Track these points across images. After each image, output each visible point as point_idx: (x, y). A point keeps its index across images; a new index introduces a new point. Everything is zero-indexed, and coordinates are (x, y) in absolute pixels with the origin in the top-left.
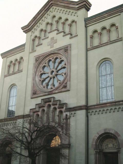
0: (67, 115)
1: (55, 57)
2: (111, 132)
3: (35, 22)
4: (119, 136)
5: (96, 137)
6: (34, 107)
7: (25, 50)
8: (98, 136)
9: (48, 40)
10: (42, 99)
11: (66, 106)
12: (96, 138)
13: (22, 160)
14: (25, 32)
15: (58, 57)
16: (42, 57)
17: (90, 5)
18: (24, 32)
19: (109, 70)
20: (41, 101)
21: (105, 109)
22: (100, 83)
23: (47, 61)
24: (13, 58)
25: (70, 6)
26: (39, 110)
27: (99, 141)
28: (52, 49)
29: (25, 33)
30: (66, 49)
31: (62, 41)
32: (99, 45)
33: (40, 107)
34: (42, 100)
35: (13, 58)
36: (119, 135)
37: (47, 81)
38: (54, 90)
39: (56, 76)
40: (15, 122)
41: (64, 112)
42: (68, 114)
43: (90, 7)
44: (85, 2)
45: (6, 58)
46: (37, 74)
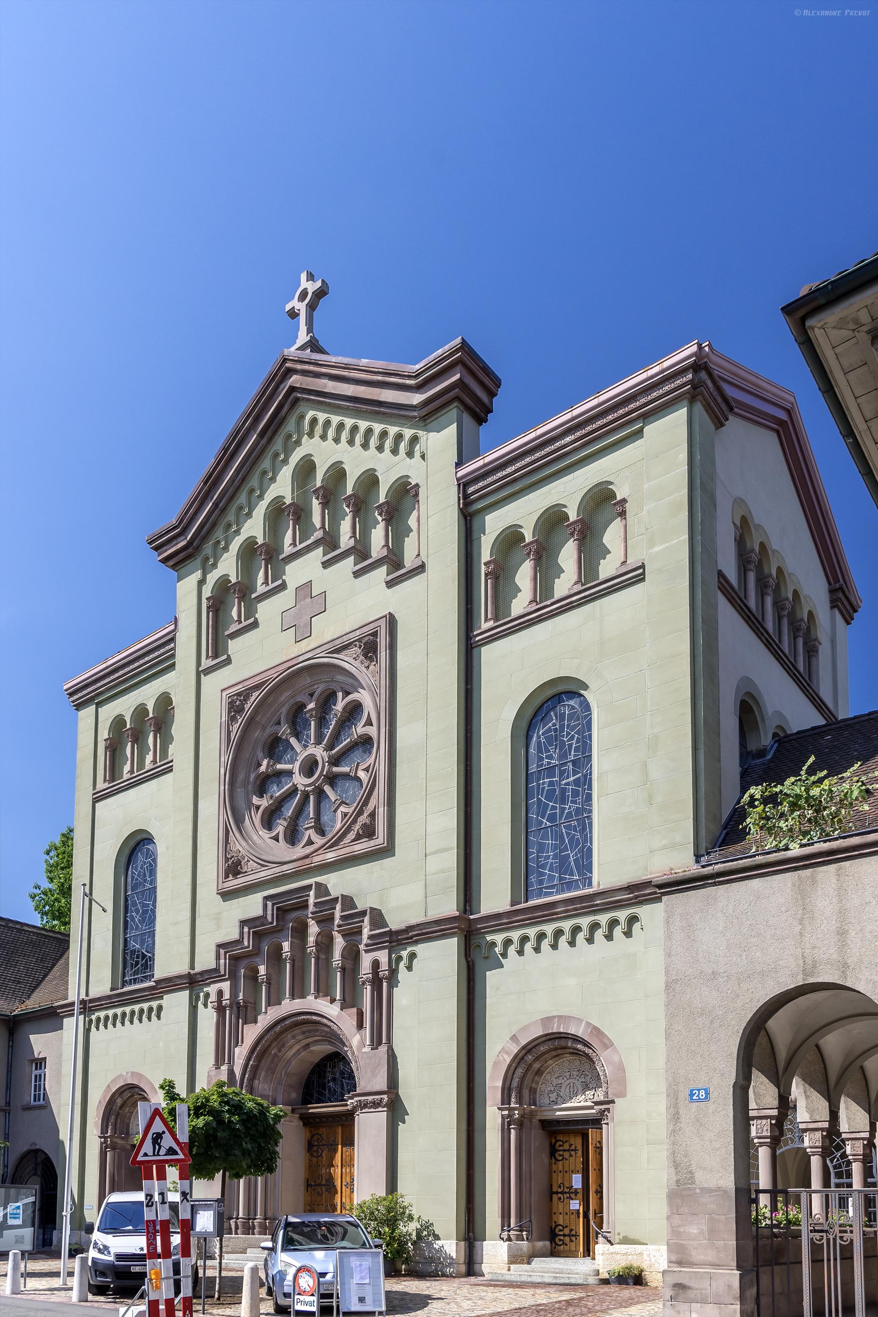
0: (376, 964)
1: (319, 689)
2: (572, 1030)
3: (216, 505)
4: (608, 1044)
5: (507, 1053)
6: (235, 936)
7: (178, 659)
8: (515, 1049)
9: (284, 600)
10: (76, 835)
11: (374, 925)
12: (508, 1061)
13: (229, 1250)
14: (171, 563)
15: (334, 686)
16: (257, 693)
17: (498, 383)
18: (164, 561)
19: (572, 738)
20: (265, 907)
21: (549, 929)
22: (530, 807)
23: (284, 710)
24: (124, 706)
25: (382, 398)
26: (259, 948)
27: (520, 1071)
28: (304, 646)
29: (173, 567)
30: (376, 642)
31: (352, 600)
32: (529, 609)
33: (258, 936)
34: (266, 898)
35: (124, 706)
36: (606, 1040)
37: (289, 810)
38: (320, 852)
39: (333, 785)
40: (154, 1004)
41: (366, 951)
42: (383, 956)
43: (492, 394)
44: (224, 694)
45: (93, 707)
46: (241, 777)
